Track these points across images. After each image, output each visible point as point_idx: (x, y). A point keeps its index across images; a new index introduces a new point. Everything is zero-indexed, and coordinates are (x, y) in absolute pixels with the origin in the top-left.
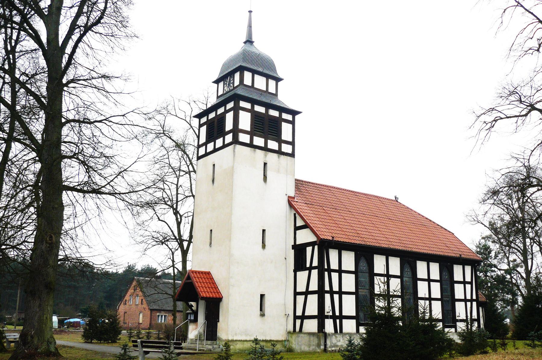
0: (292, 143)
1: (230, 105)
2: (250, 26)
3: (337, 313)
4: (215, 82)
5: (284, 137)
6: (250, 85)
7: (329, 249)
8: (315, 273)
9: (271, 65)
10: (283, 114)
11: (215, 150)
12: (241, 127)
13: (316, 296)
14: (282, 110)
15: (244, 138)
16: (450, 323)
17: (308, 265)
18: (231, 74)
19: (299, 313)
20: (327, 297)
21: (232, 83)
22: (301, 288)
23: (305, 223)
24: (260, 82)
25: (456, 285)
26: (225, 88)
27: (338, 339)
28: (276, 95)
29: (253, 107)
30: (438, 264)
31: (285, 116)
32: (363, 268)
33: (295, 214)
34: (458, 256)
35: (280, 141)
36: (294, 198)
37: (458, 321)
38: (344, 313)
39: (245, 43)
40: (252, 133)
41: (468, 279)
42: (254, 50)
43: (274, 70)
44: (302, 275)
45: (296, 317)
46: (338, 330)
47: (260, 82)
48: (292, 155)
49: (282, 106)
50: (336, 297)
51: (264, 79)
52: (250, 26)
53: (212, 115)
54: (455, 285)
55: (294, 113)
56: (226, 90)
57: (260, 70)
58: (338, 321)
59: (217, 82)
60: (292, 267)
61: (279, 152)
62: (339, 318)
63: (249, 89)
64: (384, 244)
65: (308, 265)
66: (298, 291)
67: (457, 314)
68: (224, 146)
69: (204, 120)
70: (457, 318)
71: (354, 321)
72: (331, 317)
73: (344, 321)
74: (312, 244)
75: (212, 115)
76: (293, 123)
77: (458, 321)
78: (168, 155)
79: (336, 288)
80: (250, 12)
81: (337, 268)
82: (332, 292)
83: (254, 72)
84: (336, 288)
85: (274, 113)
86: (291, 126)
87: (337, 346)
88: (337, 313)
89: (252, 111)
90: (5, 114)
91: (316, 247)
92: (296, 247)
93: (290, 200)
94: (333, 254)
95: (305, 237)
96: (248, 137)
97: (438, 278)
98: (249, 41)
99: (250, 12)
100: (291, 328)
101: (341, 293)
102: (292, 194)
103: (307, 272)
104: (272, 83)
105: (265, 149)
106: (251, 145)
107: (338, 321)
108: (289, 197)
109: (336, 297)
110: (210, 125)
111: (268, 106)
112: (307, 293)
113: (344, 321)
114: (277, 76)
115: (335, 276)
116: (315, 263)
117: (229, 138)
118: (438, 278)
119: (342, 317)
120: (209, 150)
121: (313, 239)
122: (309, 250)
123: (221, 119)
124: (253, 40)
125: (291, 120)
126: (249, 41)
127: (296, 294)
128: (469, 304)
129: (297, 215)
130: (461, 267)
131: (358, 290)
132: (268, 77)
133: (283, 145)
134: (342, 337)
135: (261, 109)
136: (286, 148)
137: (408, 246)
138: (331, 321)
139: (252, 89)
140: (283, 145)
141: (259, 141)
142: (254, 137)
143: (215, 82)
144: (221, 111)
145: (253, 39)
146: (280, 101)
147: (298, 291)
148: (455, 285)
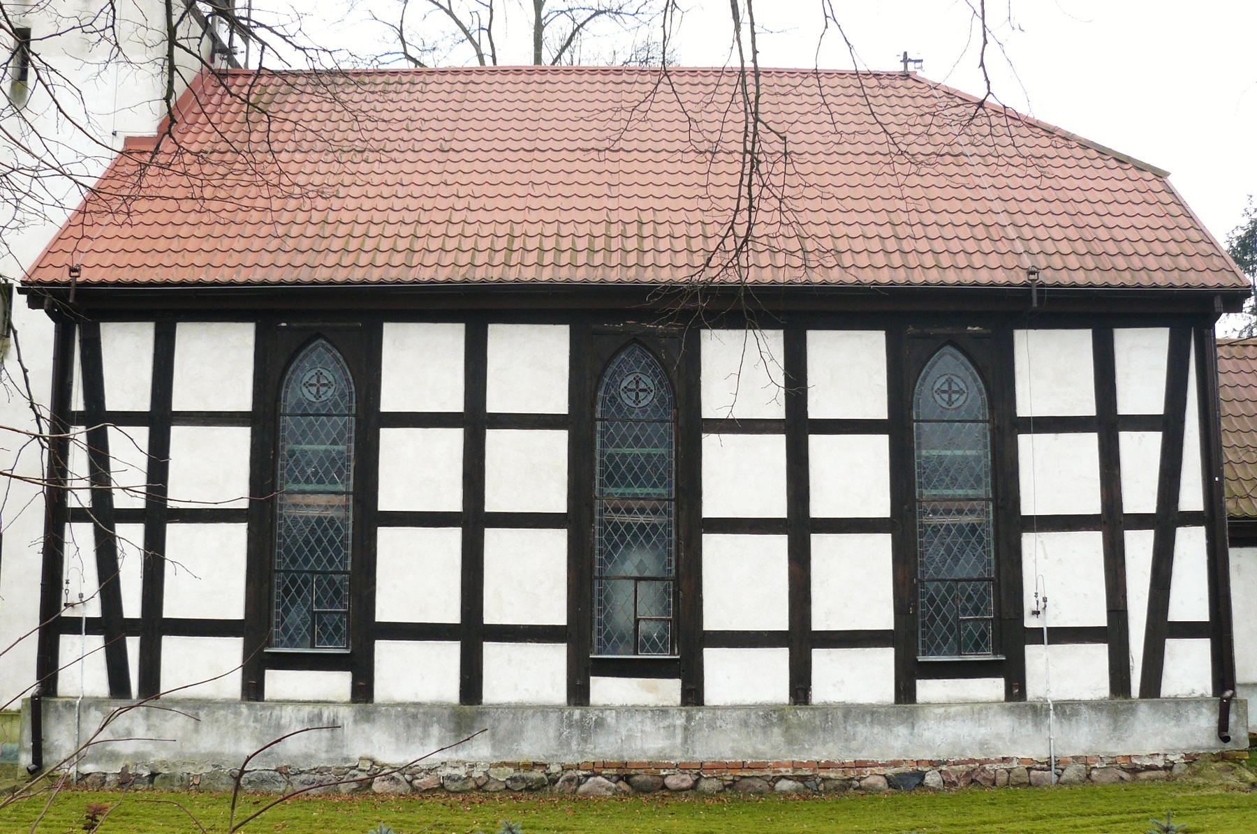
3: (132, 608)
7: (102, 325)
16: (977, 648)
20: (80, 538)
30: (565, 329)
34: (1020, 278)
37: (1036, 636)
50: (130, 537)
54: (1023, 439)
58: (133, 645)
67: (1029, 603)
70: (1030, 622)
71: (885, 657)
72: (93, 626)
77: (1036, 636)
78: (656, 88)
87: (114, 757)
88: (132, 608)
107: (133, 645)
109: (130, 537)
148: (1023, 439)
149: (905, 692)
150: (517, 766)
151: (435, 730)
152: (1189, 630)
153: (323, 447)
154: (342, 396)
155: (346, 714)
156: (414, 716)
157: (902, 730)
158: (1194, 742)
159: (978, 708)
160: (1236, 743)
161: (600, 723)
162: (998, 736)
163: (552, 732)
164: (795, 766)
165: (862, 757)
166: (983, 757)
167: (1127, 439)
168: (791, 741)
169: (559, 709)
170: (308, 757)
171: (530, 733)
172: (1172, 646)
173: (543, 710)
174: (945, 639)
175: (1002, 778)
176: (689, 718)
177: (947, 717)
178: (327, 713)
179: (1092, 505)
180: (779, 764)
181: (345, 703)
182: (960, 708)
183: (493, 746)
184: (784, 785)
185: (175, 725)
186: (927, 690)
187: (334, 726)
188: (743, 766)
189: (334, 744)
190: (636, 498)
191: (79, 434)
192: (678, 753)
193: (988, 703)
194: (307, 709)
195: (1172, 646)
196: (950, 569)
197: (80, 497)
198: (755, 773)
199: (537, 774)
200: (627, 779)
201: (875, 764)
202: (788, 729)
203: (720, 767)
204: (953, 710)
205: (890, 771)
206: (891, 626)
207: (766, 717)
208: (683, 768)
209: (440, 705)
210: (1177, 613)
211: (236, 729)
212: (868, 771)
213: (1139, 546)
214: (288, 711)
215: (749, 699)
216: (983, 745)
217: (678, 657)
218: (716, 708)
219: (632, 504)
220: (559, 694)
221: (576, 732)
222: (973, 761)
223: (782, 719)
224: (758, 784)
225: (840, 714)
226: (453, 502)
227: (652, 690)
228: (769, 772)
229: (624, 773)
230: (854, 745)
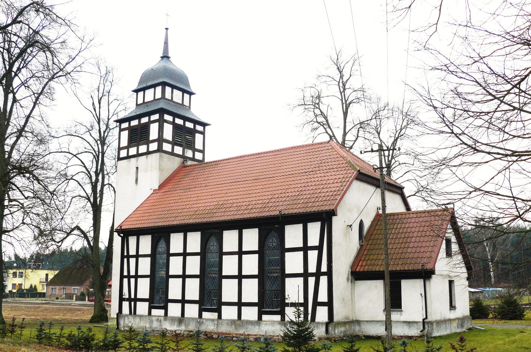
0: (203, 152)
1: (156, 117)
2: (166, 43)
3: (133, 297)
4: (134, 91)
6: (170, 99)
9: (184, 79)
10: (176, 119)
11: (138, 155)
14: (196, 122)
15: (167, 147)
20: (125, 281)
24: (177, 96)
27: (130, 320)
31: (199, 128)
32: (162, 250)
35: (194, 150)
39: (162, 58)
40: (174, 143)
42: (170, 66)
43: (188, 85)
46: (133, 312)
49: (195, 118)
50: (133, 280)
51: (181, 93)
52: (166, 43)
53: (134, 123)
55: (204, 125)
57: (178, 85)
58: (133, 303)
59: (137, 91)
62: (134, 300)
63: (179, 106)
68: (148, 153)
69: (125, 125)
70: (287, 301)
73: (138, 303)
75: (134, 123)
76: (203, 133)
77: (287, 305)
80: (167, 29)
81: (188, 251)
82: (129, 277)
83: (173, 87)
84: (133, 273)
86: (202, 136)
88: (133, 297)
89: (173, 123)
94: (132, 240)
96: (170, 146)
98: (165, 57)
99: (167, 29)
101: (137, 277)
104: (186, 96)
107: (133, 303)
110: (132, 131)
111: (186, 119)
113: (138, 303)
114: (191, 91)
115: (133, 261)
117: (154, 146)
119: (136, 300)
120: (131, 154)
123: (145, 128)
124: (169, 56)
126: (165, 57)
131: (219, 269)
132: (184, 91)
133: (197, 153)
134: (134, 318)
138: (128, 303)
139: (182, 107)
140: (197, 153)
143: (134, 91)
144: (145, 120)
146: (193, 114)
149: (260, 318)
150: (189, 331)
151: (176, 323)
152: (322, 304)
153: (277, 257)
154: (278, 244)
155: (162, 319)
156: (173, 320)
157: (257, 327)
158: (321, 334)
159: (273, 322)
160: (331, 335)
161: (203, 322)
162: (277, 330)
163: (195, 324)
164: (236, 334)
165: (249, 333)
166: (273, 335)
167: (131, 259)
168: (236, 328)
169: (196, 319)
170: (157, 328)
171: (191, 324)
172: (318, 308)
173: (193, 319)
174: (270, 305)
175: (277, 341)
176: (218, 322)
177: (266, 324)
178: (160, 318)
179: (301, 271)
180: (233, 334)
181: (163, 317)
182: (269, 322)
183: (185, 327)
184: (234, 339)
185: (138, 320)
186: (265, 317)
187: (160, 321)
188: (226, 334)
189: (161, 325)
190: (272, 270)
191: (125, 260)
192: (215, 330)
193: (275, 322)
194: (157, 317)
195: (318, 308)
196: (271, 288)
197: (125, 273)
198: (229, 335)
199: (191, 333)
200: (206, 335)
201: (252, 335)
202: (235, 326)
203: (222, 333)
204: (268, 323)
205: (254, 337)
206: (257, 302)
207: (232, 322)
208: (215, 333)
209: (177, 317)
210: (320, 300)
211: (146, 321)
212: (250, 337)
213: (312, 281)
214: (154, 317)
215: (230, 318)
216: (273, 332)
217: (105, 303)
218: (224, 320)
219: (212, 272)
220: (197, 316)
221: (198, 324)
222: (271, 336)
223: (234, 323)
224: (229, 338)
225: (245, 322)
226: (187, 273)
227: (213, 315)
228: (231, 335)
229: (206, 334)
230: (248, 330)
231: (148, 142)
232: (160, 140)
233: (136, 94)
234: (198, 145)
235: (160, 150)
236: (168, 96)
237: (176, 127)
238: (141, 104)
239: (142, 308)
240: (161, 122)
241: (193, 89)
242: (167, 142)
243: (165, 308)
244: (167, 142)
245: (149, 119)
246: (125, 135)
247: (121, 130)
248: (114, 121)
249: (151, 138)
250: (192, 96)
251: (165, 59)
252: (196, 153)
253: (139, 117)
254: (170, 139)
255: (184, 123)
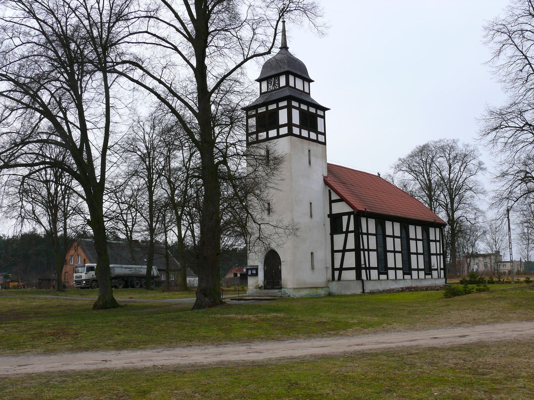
0: (324, 134)
1: (285, 103)
3: (367, 266)
5: (319, 130)
8: (351, 236)
12: (294, 122)
13: (353, 253)
15: (296, 131)
17: (344, 229)
18: (277, 76)
19: (337, 265)
21: (277, 84)
22: (339, 246)
23: (340, 197)
24: (299, 85)
25: (431, 243)
26: (270, 87)
28: (309, 94)
29: (300, 105)
31: (320, 113)
33: (329, 191)
35: (318, 133)
36: (327, 177)
38: (371, 266)
40: (278, 127)
41: (438, 239)
44: (339, 239)
45: (334, 269)
47: (299, 85)
48: (325, 144)
50: (366, 253)
55: (324, 109)
56: (271, 89)
58: (368, 271)
60: (329, 231)
61: (317, 141)
64: (392, 213)
65: (344, 229)
66: (335, 249)
68: (278, 136)
70: (432, 268)
74: (348, 214)
76: (323, 117)
79: (366, 247)
83: (296, 76)
84: (366, 247)
85: (312, 110)
88: (367, 266)
90: (455, 180)
91: (352, 216)
92: (331, 216)
93: (326, 179)
95: (339, 208)
97: (374, 232)
100: (330, 276)
102: (326, 175)
103: (344, 235)
104: (306, 84)
105: (309, 139)
106: (300, 136)
108: (324, 177)
110: (260, 118)
112: (344, 251)
114: (307, 77)
116: (352, 228)
117: (284, 131)
118: (374, 232)
121: (348, 209)
122: (345, 219)
123: (275, 114)
125: (323, 115)
127: (333, 252)
128: (438, 257)
129: (332, 191)
130: (434, 229)
135: (304, 107)
136: (321, 138)
137: (403, 214)
141: (305, 133)
142: (287, 127)
145: (288, 46)
146: (312, 100)
147: (335, 249)
231: (278, 127)
232: (290, 125)
233: (259, 83)
234: (320, 129)
235: (290, 133)
236: (292, 84)
237: (302, 112)
238: (265, 93)
239: (374, 274)
240: (289, 108)
241: (311, 76)
242: (296, 126)
243: (387, 274)
244: (296, 126)
245: (277, 105)
246: (253, 121)
247: (248, 117)
248: (330, 109)
249: (281, 122)
250: (311, 83)
251: (284, 49)
252: (319, 135)
253: (266, 104)
254: (298, 124)
255: (308, 109)
